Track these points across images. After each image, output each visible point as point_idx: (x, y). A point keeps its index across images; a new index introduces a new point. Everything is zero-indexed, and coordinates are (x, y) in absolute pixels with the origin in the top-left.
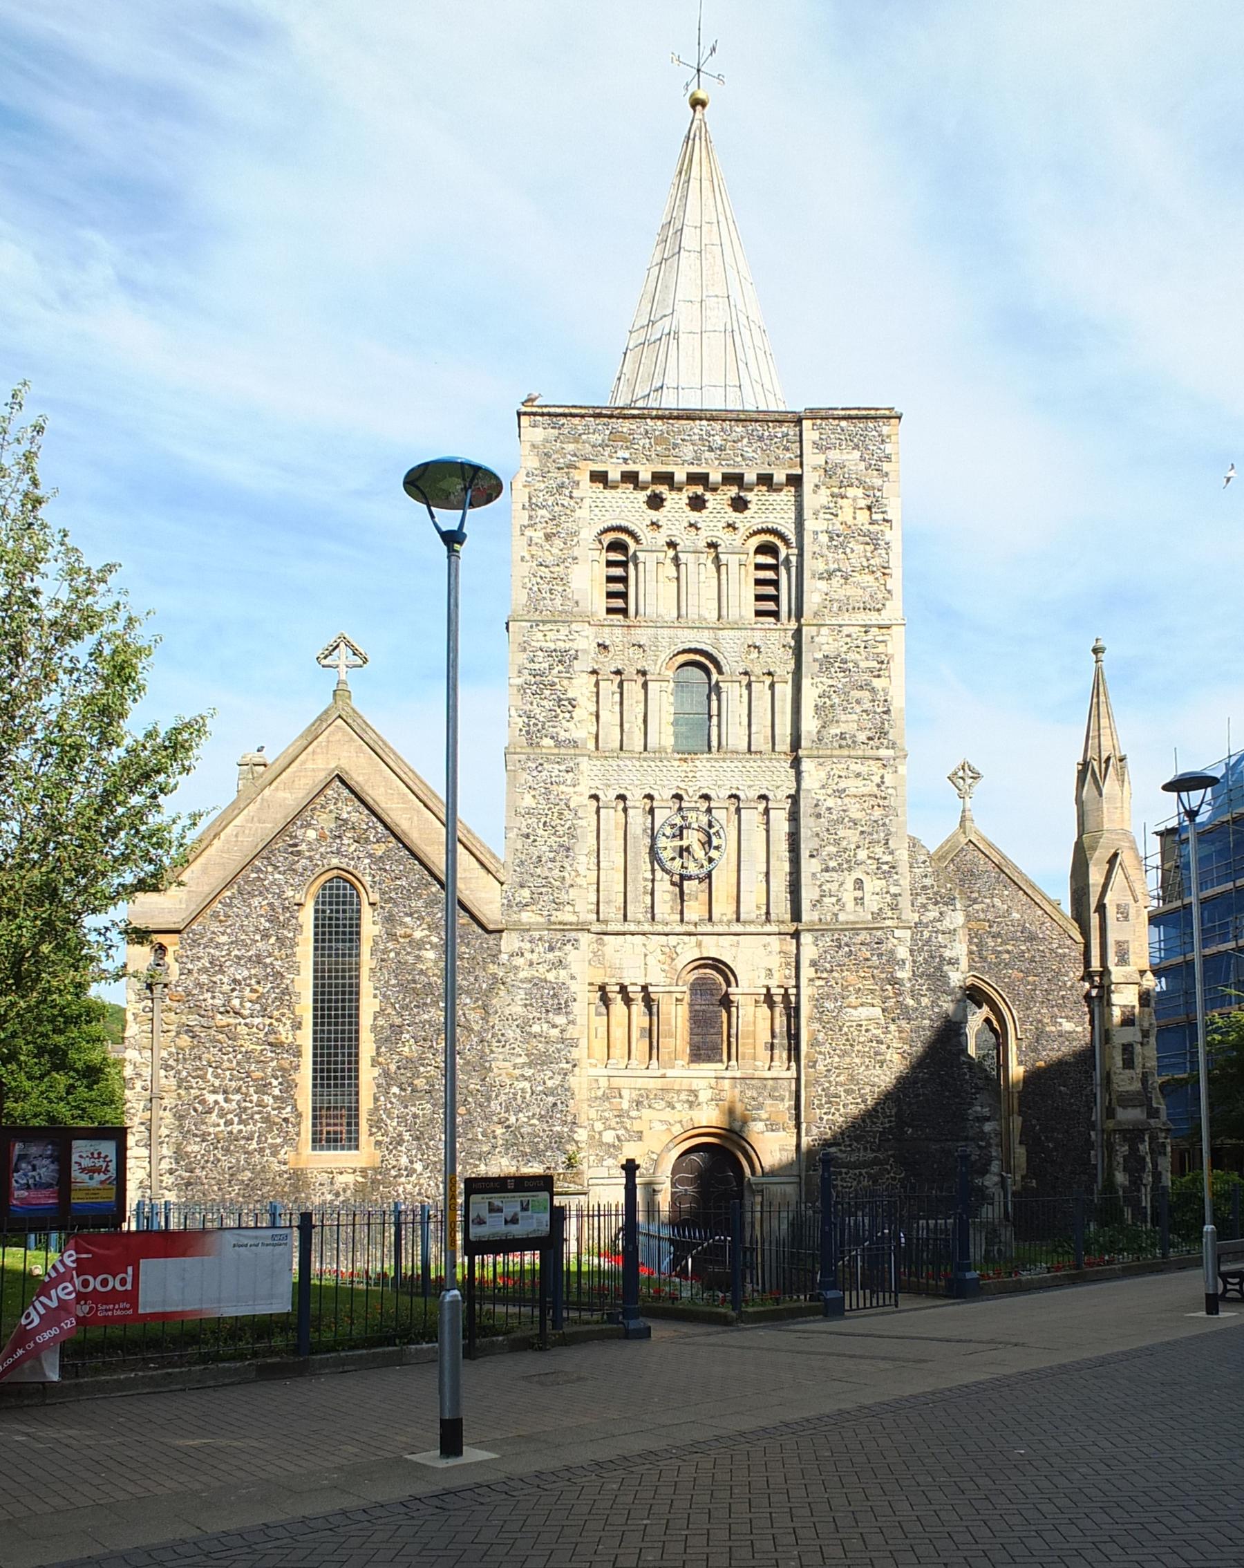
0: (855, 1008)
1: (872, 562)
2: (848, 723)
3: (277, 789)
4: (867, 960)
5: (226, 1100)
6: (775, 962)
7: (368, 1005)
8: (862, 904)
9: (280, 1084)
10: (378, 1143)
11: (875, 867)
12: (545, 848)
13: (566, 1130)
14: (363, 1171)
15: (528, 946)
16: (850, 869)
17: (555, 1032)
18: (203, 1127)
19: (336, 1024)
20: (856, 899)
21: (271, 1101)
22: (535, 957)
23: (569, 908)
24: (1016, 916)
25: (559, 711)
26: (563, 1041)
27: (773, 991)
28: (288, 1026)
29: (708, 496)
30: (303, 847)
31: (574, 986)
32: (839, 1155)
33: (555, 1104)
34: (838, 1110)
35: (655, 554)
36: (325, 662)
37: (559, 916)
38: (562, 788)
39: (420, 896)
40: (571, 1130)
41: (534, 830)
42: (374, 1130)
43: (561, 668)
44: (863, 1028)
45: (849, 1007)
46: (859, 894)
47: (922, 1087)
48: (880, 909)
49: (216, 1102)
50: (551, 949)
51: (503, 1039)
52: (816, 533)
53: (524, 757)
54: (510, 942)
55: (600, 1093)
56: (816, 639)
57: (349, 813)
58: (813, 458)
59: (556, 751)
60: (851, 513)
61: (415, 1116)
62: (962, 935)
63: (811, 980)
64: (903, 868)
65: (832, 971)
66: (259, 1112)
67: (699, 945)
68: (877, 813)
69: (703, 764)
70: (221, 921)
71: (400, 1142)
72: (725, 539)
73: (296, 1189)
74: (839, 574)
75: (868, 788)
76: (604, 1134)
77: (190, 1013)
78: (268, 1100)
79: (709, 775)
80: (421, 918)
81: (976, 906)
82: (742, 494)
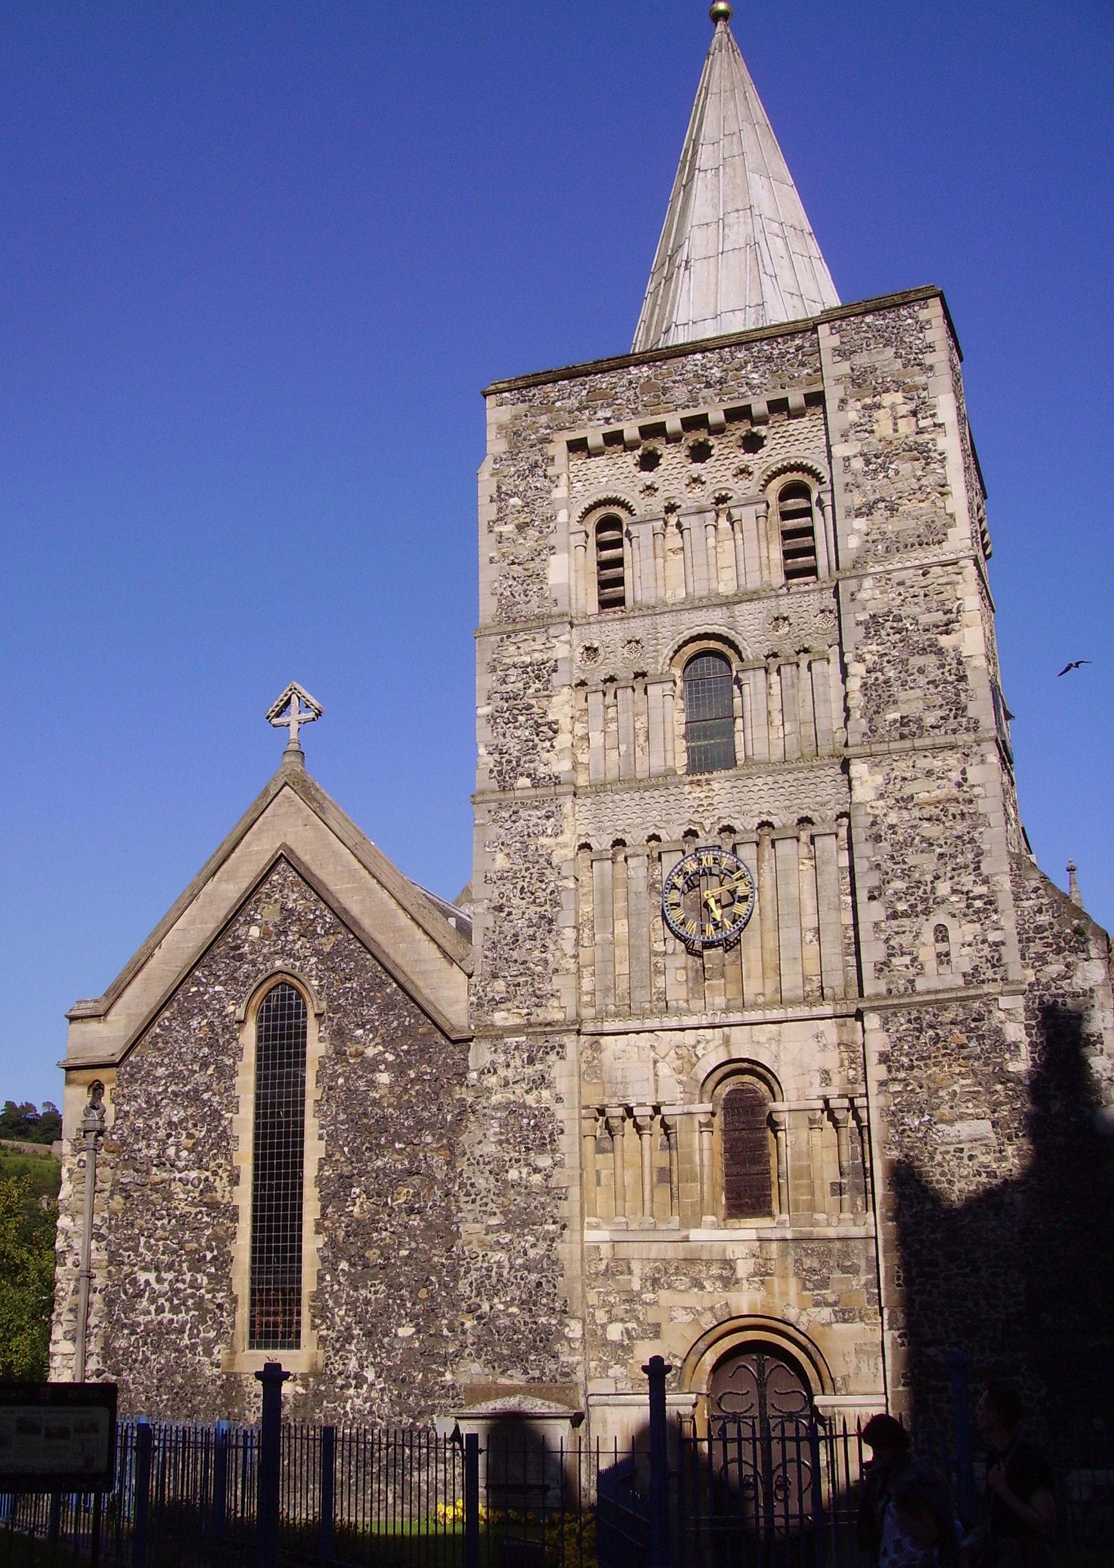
0: (950, 1122)
1: (924, 482)
2: (909, 702)
3: (220, 880)
4: (962, 1046)
5: (159, 1280)
6: (831, 1059)
7: (313, 1149)
9: (215, 1258)
10: (322, 1340)
11: (962, 905)
12: (520, 923)
13: (554, 1322)
15: (501, 1058)
16: (927, 912)
17: (537, 1179)
18: (132, 1315)
19: (279, 1176)
20: (939, 955)
21: (206, 1280)
22: (510, 1074)
23: (554, 1002)
25: (536, 739)
26: (548, 1191)
27: (833, 1103)
28: (225, 1180)
29: (712, 441)
30: (246, 948)
31: (561, 1112)
33: (539, 1284)
35: (650, 525)
36: (276, 721)
37: (541, 1015)
38: (543, 840)
39: (373, 1000)
40: (561, 1323)
41: (509, 900)
42: (318, 1321)
43: (538, 685)
44: (965, 1154)
45: (942, 1121)
46: (942, 947)
48: (976, 968)
49: (147, 1282)
50: (531, 1061)
51: (473, 1191)
52: (847, 459)
53: (493, 806)
54: (480, 1055)
56: (859, 596)
57: (295, 901)
58: (835, 369)
59: (532, 792)
60: (891, 421)
61: (367, 1302)
63: (882, 1084)
64: (1005, 900)
65: (912, 1068)
66: (193, 1296)
67: (727, 1041)
68: (960, 827)
69: (720, 783)
70: (159, 1049)
71: (349, 1338)
72: (740, 489)
73: (229, 1402)
74: (882, 505)
75: (946, 790)
76: (610, 1328)
77: (126, 1167)
78: (203, 1279)
79: (722, 799)
80: (374, 1030)
82: (755, 430)
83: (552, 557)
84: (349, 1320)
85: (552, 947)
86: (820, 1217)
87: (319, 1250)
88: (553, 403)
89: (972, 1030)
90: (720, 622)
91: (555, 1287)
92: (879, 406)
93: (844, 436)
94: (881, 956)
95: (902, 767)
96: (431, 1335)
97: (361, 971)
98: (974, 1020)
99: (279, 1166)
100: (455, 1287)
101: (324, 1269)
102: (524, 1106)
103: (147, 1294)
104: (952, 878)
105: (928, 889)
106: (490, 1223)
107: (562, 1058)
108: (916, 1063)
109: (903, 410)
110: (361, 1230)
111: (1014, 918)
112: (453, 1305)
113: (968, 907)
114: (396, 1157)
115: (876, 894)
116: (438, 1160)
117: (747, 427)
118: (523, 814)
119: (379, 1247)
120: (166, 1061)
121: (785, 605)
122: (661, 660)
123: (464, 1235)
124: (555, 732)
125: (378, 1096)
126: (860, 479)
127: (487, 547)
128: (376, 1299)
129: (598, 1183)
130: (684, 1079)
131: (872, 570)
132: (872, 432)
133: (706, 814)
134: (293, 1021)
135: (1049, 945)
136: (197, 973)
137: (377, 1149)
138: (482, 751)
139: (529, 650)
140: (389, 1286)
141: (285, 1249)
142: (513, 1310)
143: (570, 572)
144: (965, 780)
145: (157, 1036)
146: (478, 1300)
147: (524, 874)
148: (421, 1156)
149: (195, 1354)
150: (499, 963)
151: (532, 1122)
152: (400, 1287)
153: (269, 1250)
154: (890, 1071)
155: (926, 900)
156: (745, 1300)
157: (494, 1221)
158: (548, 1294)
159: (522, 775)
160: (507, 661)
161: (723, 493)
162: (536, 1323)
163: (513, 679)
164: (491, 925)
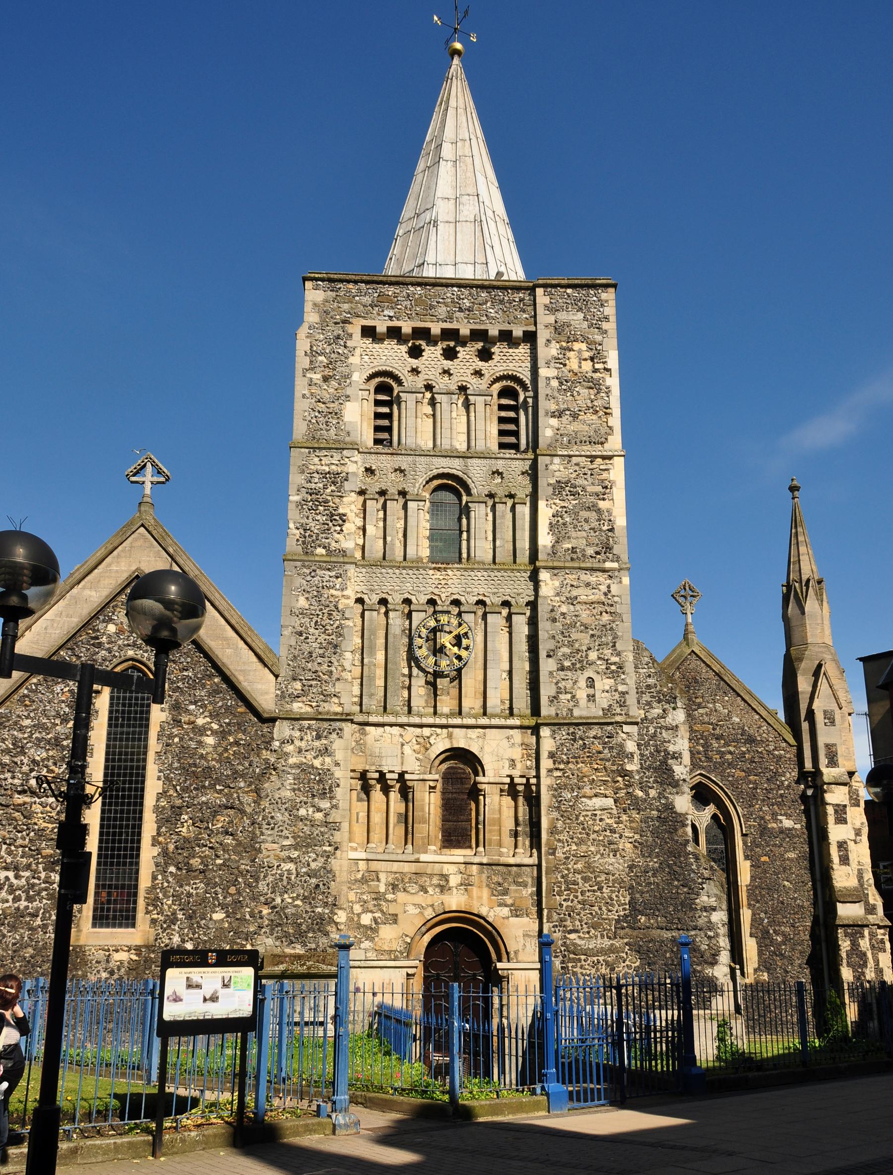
0: (590, 798)
1: (595, 403)
2: (578, 539)
3: (84, 588)
4: (600, 752)
5: (17, 877)
6: (517, 753)
7: (153, 786)
8: (594, 701)
10: (154, 922)
11: (604, 667)
14: (138, 949)
15: (297, 734)
16: (582, 669)
17: (319, 816)
20: (588, 696)
22: (303, 744)
23: (335, 700)
24: (736, 720)
25: (331, 524)
31: (338, 773)
32: (579, 942)
33: (317, 886)
34: (577, 897)
38: (332, 592)
39: (204, 686)
41: (307, 628)
43: (333, 488)
44: (598, 818)
45: (584, 797)
46: (591, 691)
47: (654, 875)
49: (7, 878)
50: (318, 737)
51: (272, 821)
52: (548, 379)
55: (359, 876)
56: (551, 467)
58: (545, 319)
61: (189, 895)
62: (684, 731)
63: (550, 771)
64: (629, 667)
65: (568, 763)
66: (46, 889)
67: (450, 736)
70: (26, 706)
72: (474, 384)
76: (363, 916)
79: (453, 583)
80: (204, 706)
81: (701, 711)
83: (348, 403)
84: (175, 907)
85: (336, 664)
86: (504, 850)
87: (154, 857)
88: (354, 297)
89: (606, 743)
90: (458, 468)
91: (329, 888)
92: (571, 350)
93: (548, 363)
94: (553, 692)
95: (571, 578)
96: (237, 919)
97: (195, 665)
98: (608, 737)
99: (123, 797)
100: (257, 886)
101: (158, 871)
102: (312, 767)
103: (6, 887)
104: (598, 650)
105: (584, 655)
106: (284, 843)
107: (341, 737)
108: (571, 760)
109: (587, 355)
110: (186, 845)
111: (634, 678)
112: (254, 899)
113: (607, 669)
114: (217, 795)
115: (551, 654)
116: (248, 799)
117: (485, 343)
118: (319, 572)
119: (200, 857)
120: (32, 715)
121: (500, 465)
122: (417, 485)
123: (264, 851)
124: (344, 521)
125: (204, 753)
126: (556, 394)
127: (301, 387)
128: (197, 893)
129: (357, 822)
130: (421, 757)
131: (560, 453)
132: (565, 365)
133: (443, 590)
134: (125, 729)
135: (653, 697)
136: (62, 653)
137: (201, 788)
138: (291, 525)
139: (327, 462)
140: (207, 885)
141: (125, 856)
142: (298, 902)
143: (358, 415)
144: (609, 591)
145: (25, 696)
146: (272, 896)
147: (318, 612)
148: (235, 795)
149: (46, 933)
150: (297, 670)
151: (317, 778)
152: (216, 885)
153: (112, 857)
154: (554, 764)
155: (583, 661)
156: (455, 901)
157: (287, 843)
158: (324, 893)
159: (320, 546)
160: (312, 467)
161: (464, 384)
162: (313, 912)
163: (316, 480)
164: (293, 643)
